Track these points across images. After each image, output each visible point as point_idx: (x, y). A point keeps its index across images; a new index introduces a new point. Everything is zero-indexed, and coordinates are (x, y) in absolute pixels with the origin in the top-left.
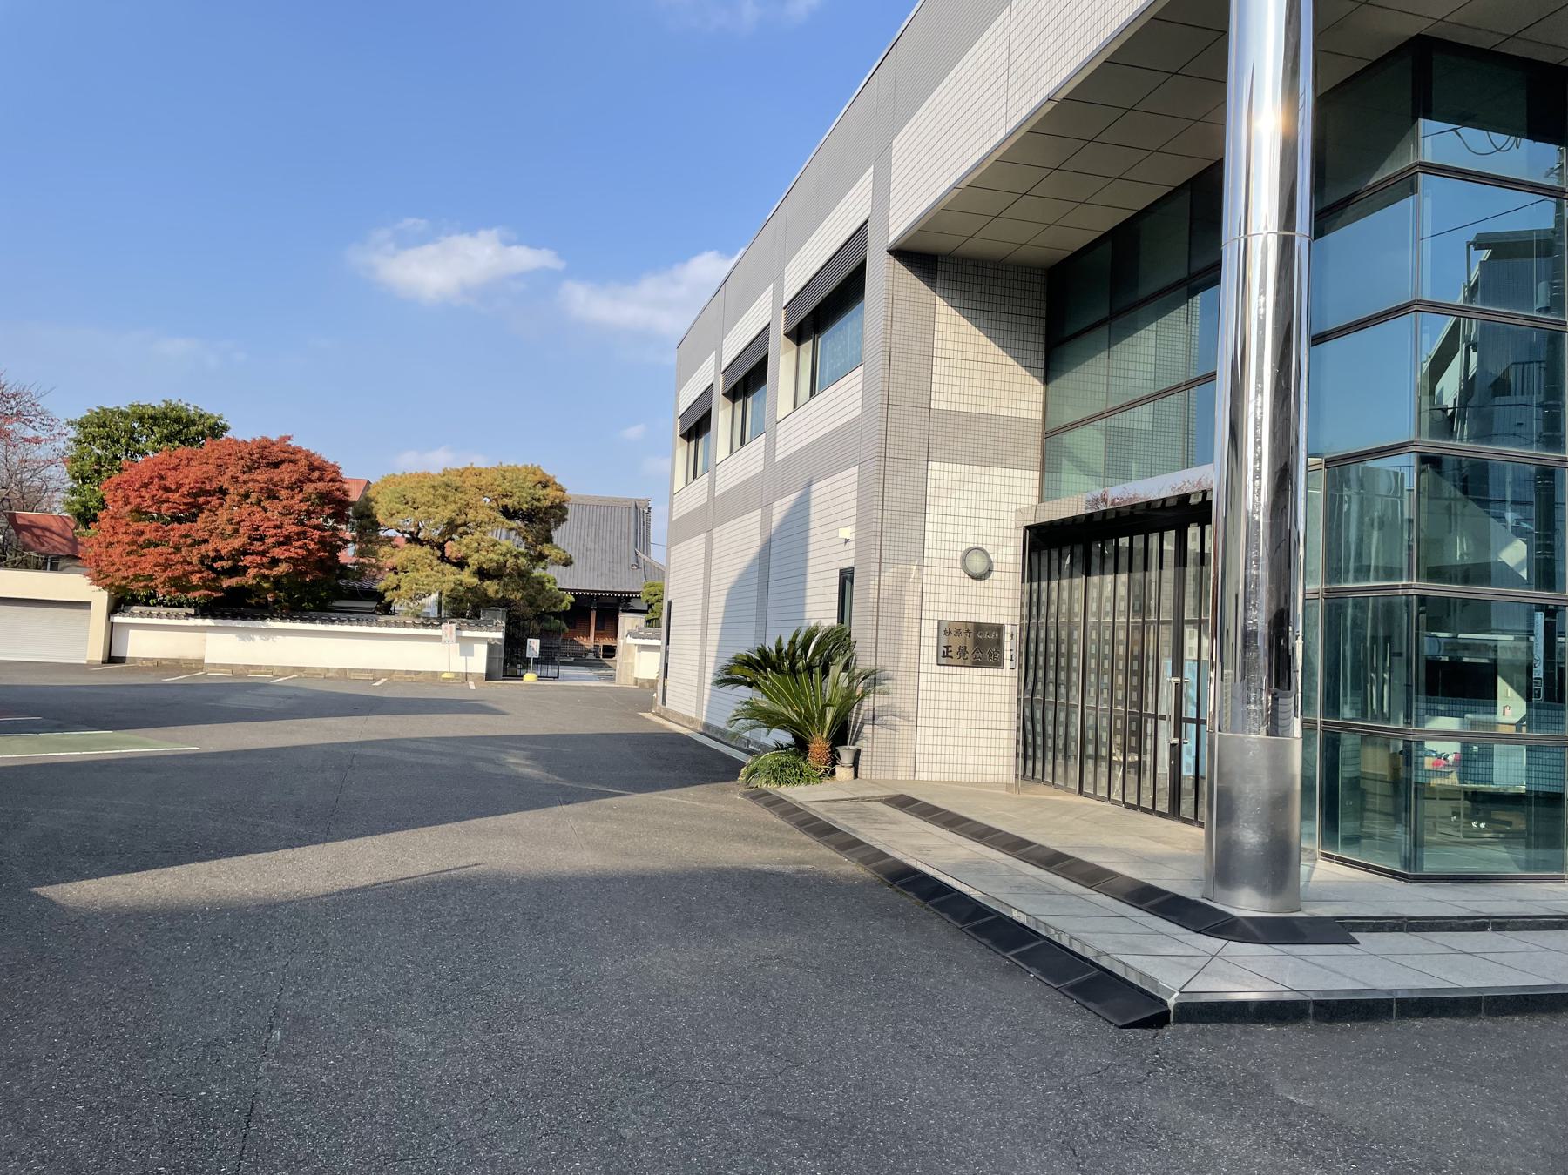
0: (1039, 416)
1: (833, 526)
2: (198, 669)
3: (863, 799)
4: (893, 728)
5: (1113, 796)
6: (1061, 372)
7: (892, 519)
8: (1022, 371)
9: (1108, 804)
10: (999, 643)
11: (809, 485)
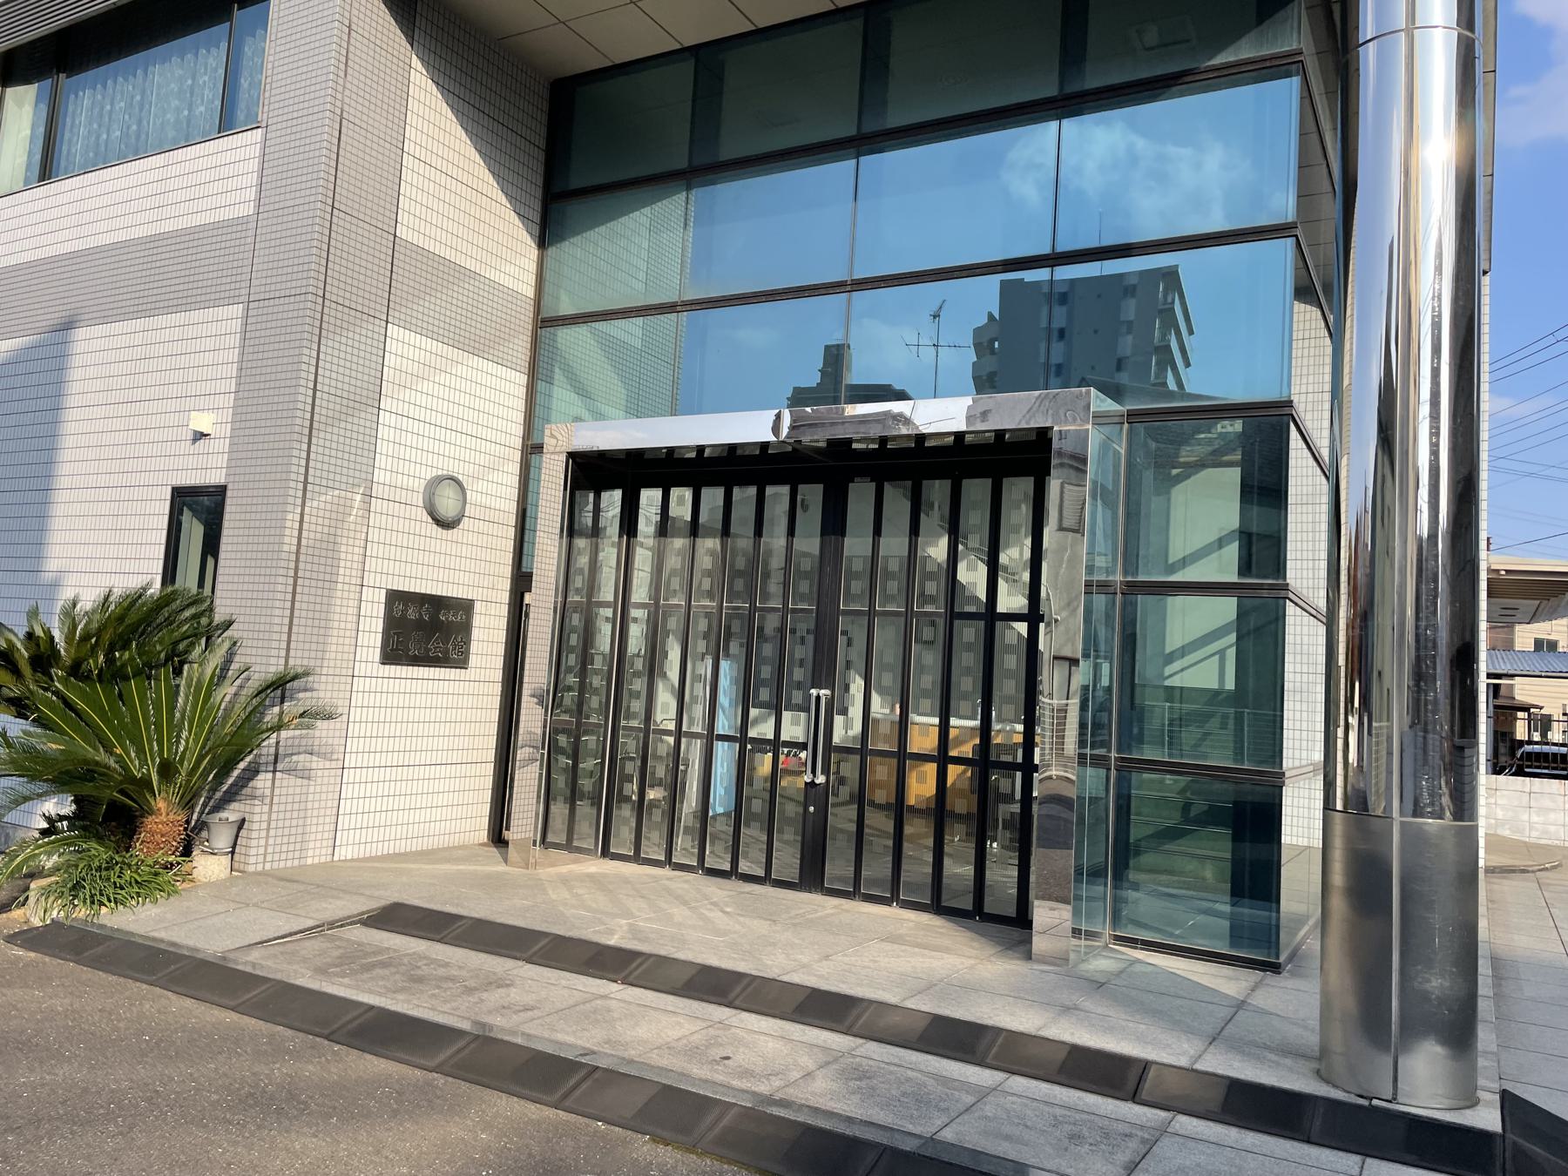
0: (530, 292)
1: (189, 403)
2: (1104, 707)
3: (332, 925)
4: (305, 774)
5: (744, 866)
6: (560, 237)
7: (302, 401)
8: (517, 221)
9: (666, 872)
10: (464, 629)
11: (68, 326)
